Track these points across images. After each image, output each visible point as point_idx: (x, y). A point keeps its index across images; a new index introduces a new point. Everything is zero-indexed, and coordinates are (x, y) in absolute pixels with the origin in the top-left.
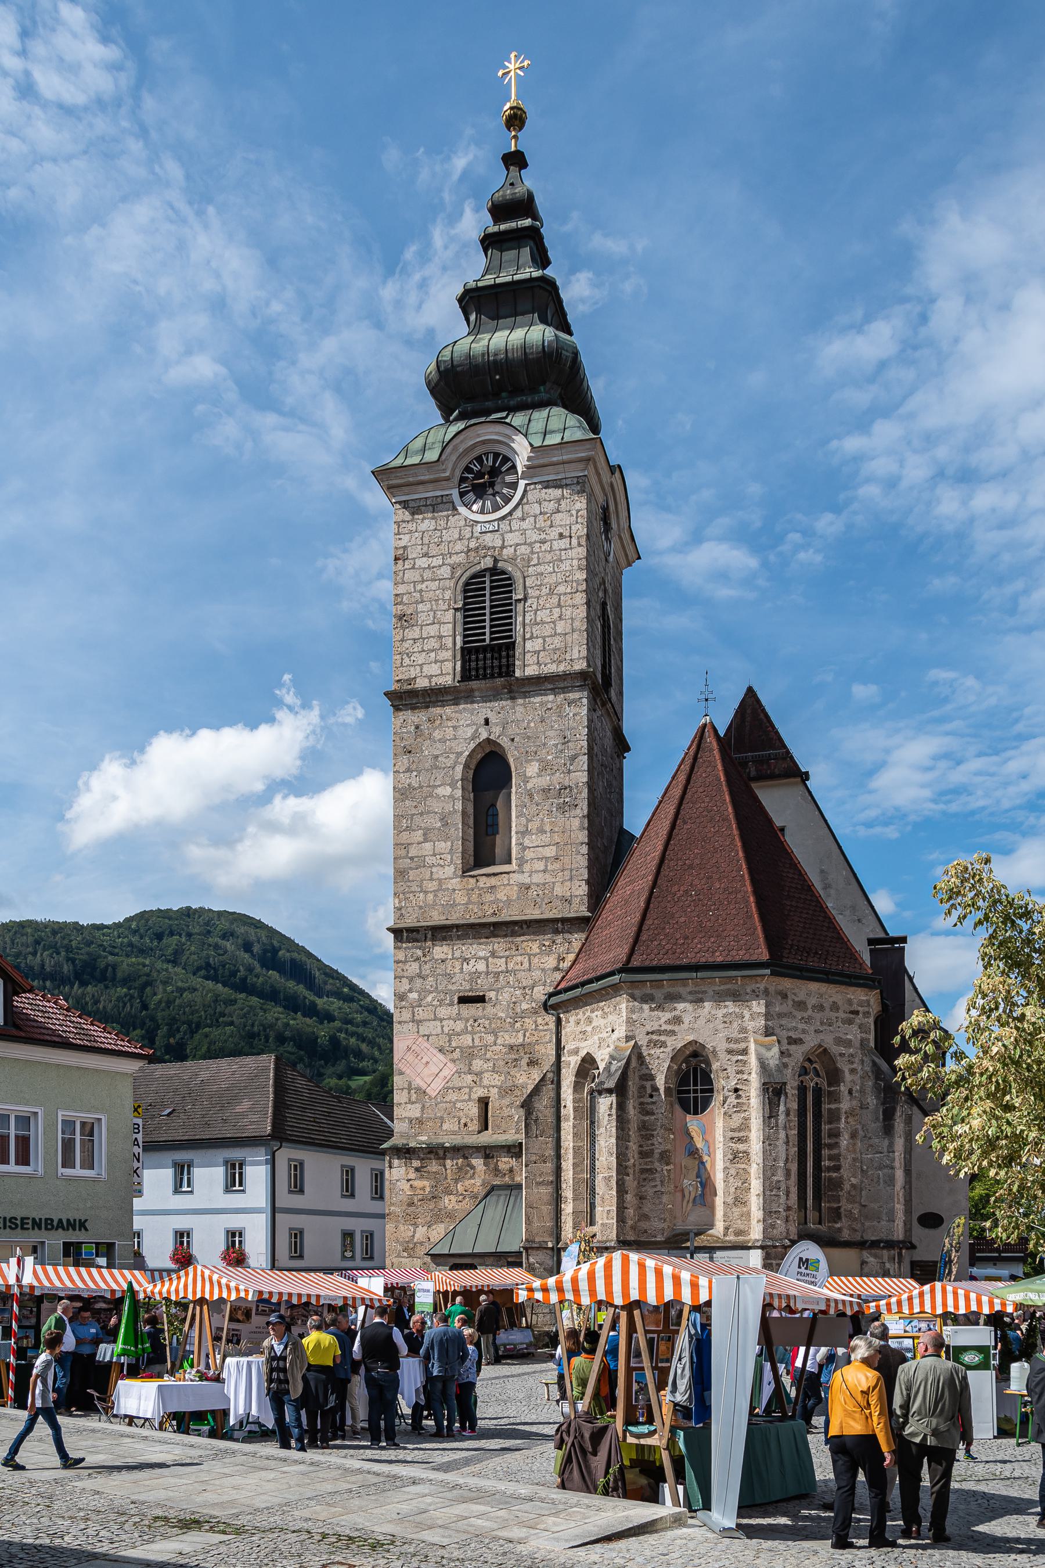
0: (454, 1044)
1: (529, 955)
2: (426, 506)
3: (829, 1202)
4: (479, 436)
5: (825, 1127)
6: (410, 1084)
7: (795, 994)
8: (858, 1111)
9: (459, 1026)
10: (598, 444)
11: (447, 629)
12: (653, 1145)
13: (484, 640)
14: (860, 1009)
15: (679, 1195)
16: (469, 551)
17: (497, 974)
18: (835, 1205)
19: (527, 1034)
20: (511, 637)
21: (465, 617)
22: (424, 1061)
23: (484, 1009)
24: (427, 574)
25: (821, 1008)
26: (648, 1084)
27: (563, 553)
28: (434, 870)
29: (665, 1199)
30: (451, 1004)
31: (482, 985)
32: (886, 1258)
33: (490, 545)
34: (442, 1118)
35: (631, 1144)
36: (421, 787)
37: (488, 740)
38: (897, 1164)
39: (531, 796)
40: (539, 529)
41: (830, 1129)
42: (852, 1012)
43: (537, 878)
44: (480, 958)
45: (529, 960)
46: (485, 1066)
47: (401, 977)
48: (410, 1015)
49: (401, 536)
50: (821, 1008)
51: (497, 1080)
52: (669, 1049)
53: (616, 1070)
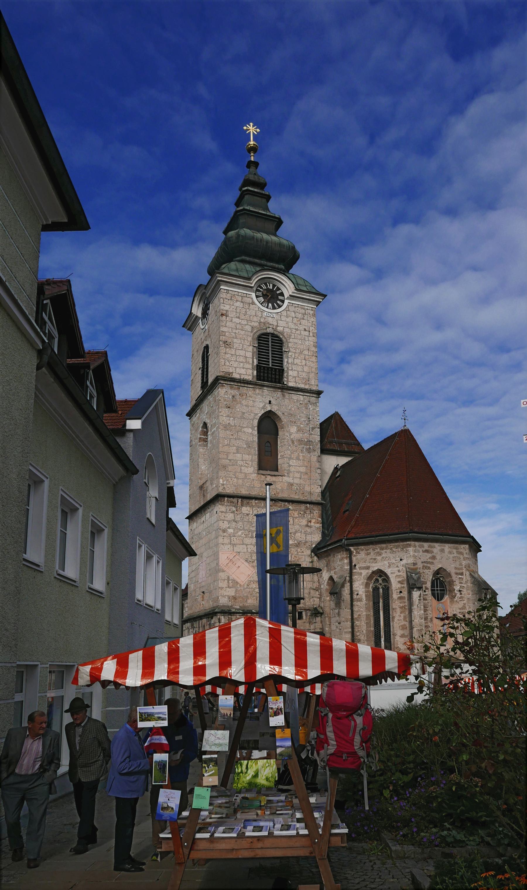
6: (228, 577)
11: (249, 355)
43: (297, 481)
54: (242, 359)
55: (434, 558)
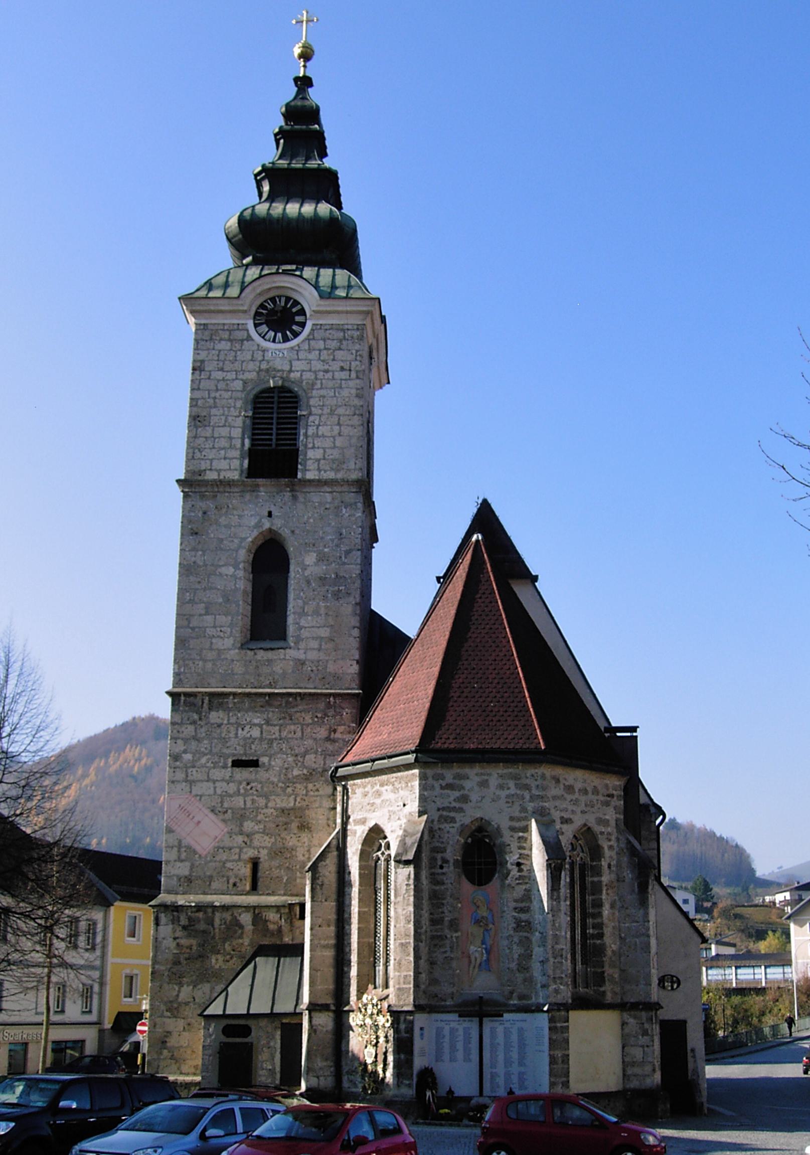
0: (226, 805)
1: (302, 725)
2: (223, 330)
3: (594, 967)
4: (275, 282)
5: (589, 898)
6: (180, 841)
7: (565, 779)
8: (615, 884)
9: (232, 788)
10: (377, 303)
11: (237, 433)
12: (443, 912)
13: (271, 445)
14: (614, 792)
15: (466, 960)
16: (260, 370)
17: (271, 742)
18: (600, 970)
19: (298, 799)
20: (295, 445)
21: (254, 424)
22: (196, 820)
23: (257, 773)
24: (221, 385)
25: (585, 792)
26: (439, 856)
27: (343, 382)
28: (214, 641)
29: (454, 964)
30: (225, 767)
31: (255, 751)
32: (644, 1019)
33: (280, 368)
34: (211, 877)
35: (424, 912)
36: (206, 565)
37: (270, 530)
38: (651, 932)
39: (308, 582)
40: (323, 361)
41: (593, 900)
42: (608, 796)
43: (312, 655)
44: (255, 725)
45: (302, 729)
46: (256, 828)
47: (176, 739)
48: (183, 776)
49: (200, 352)
50: (585, 792)
51: (268, 841)
52: (457, 825)
53: (413, 843)
54: (224, 443)
55: (465, 799)
